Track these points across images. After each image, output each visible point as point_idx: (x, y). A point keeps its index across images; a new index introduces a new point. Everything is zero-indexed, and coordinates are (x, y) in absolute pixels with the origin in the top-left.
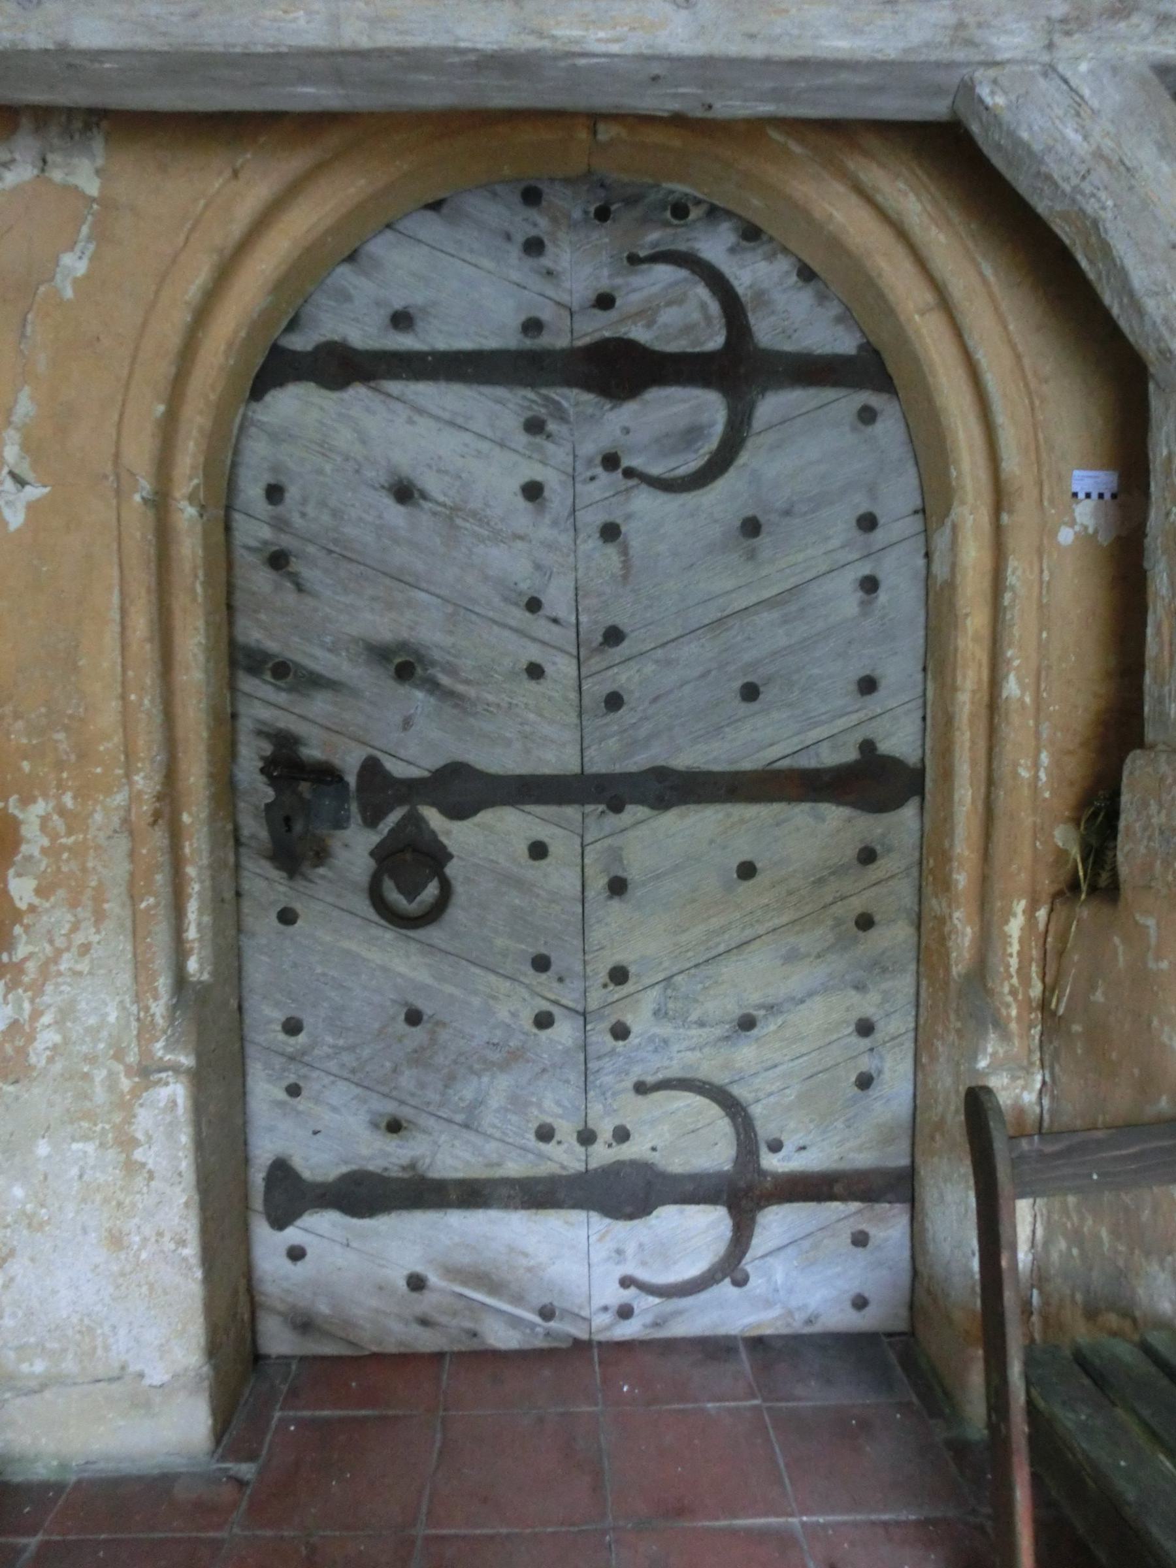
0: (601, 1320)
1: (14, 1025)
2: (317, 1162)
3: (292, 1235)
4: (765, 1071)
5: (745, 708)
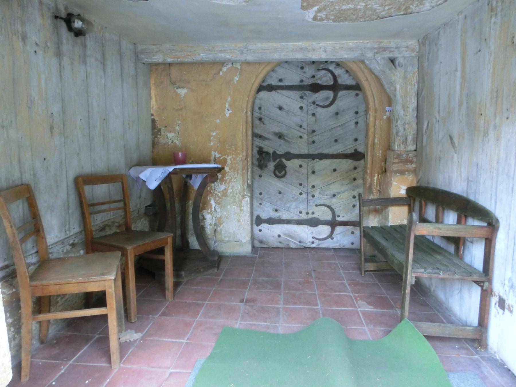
0: (309, 244)
1: (225, 188)
2: (264, 216)
3: (260, 227)
4: (337, 203)
5: (335, 143)
